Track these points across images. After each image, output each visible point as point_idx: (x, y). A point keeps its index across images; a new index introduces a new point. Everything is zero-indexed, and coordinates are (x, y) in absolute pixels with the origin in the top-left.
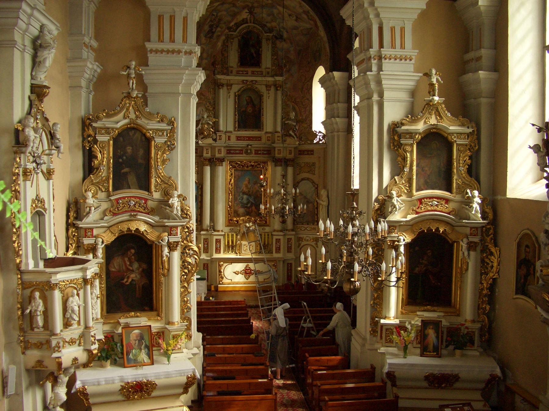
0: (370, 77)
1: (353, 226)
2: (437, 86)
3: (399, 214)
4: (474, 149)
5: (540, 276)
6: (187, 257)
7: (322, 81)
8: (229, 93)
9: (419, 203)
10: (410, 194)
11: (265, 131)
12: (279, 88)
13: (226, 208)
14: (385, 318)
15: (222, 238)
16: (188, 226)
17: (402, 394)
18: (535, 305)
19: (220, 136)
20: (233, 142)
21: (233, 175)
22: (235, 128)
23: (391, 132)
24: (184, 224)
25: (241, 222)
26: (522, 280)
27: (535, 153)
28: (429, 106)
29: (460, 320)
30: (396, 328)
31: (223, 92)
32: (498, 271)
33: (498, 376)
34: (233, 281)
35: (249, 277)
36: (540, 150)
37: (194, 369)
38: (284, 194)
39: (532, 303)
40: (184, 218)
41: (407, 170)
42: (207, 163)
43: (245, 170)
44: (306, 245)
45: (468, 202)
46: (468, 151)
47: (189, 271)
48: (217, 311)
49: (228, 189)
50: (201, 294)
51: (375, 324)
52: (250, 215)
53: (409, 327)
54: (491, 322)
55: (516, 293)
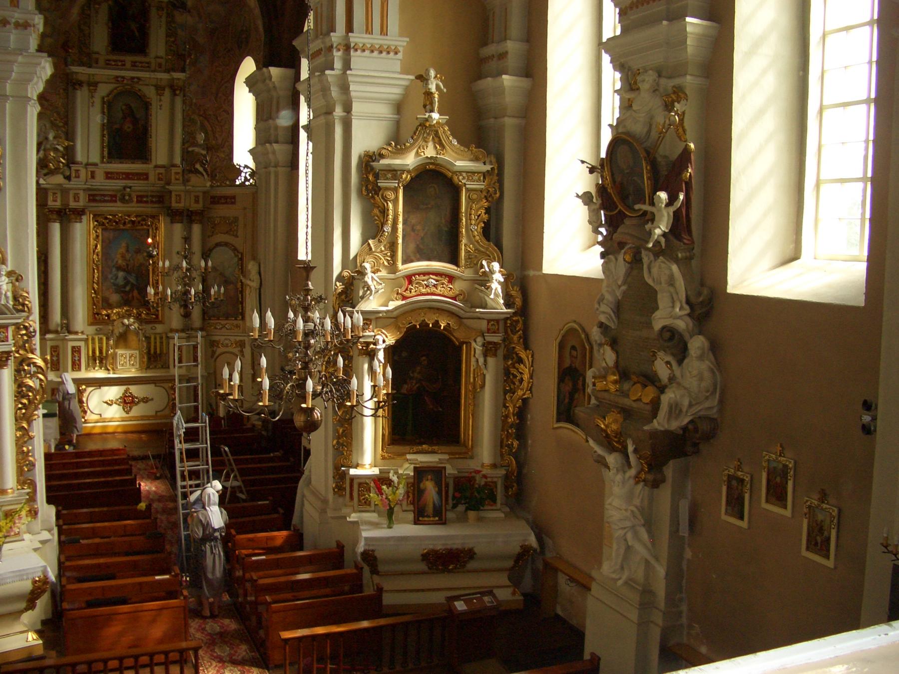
0: (330, 79)
1: (307, 320)
2: (436, 96)
3: (376, 300)
4: (493, 198)
5: (592, 392)
6: (25, 377)
7: (251, 82)
8: (92, 97)
9: (407, 283)
10: (392, 267)
11: (154, 163)
12: (178, 92)
13: (89, 294)
14: (357, 466)
15: (82, 344)
16: (27, 324)
17: (387, 585)
18: (584, 437)
19: (77, 171)
20: (100, 181)
21: (100, 237)
22: (103, 157)
23: (363, 169)
24: (20, 321)
25: (115, 318)
26: (567, 400)
27: (585, 204)
28: (424, 126)
29: (473, 465)
30: (374, 481)
31: (81, 96)
32: (531, 387)
33: (532, 547)
34: (103, 416)
35: (131, 408)
36: (591, 201)
37: (45, 567)
38: (187, 270)
39: (582, 434)
40: (18, 311)
41: (388, 229)
42: (55, 217)
43: (120, 230)
44: (224, 353)
45: (484, 280)
46: (485, 201)
47: (29, 400)
48: (77, 468)
49: (91, 262)
50: (50, 440)
51: (341, 476)
52: (130, 306)
53: (395, 479)
54: (520, 466)
55: (558, 421)
